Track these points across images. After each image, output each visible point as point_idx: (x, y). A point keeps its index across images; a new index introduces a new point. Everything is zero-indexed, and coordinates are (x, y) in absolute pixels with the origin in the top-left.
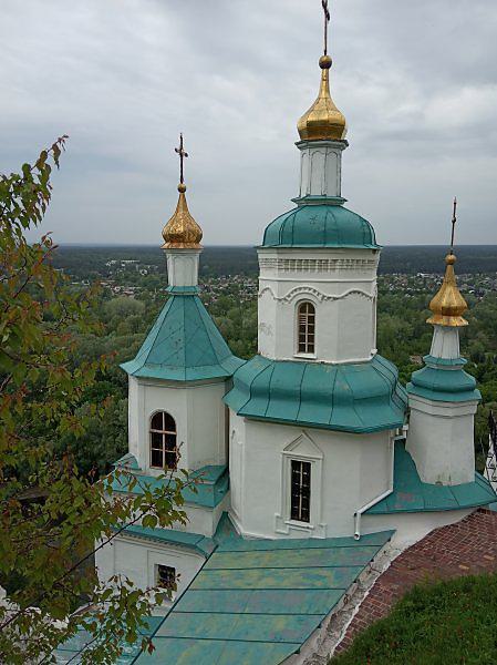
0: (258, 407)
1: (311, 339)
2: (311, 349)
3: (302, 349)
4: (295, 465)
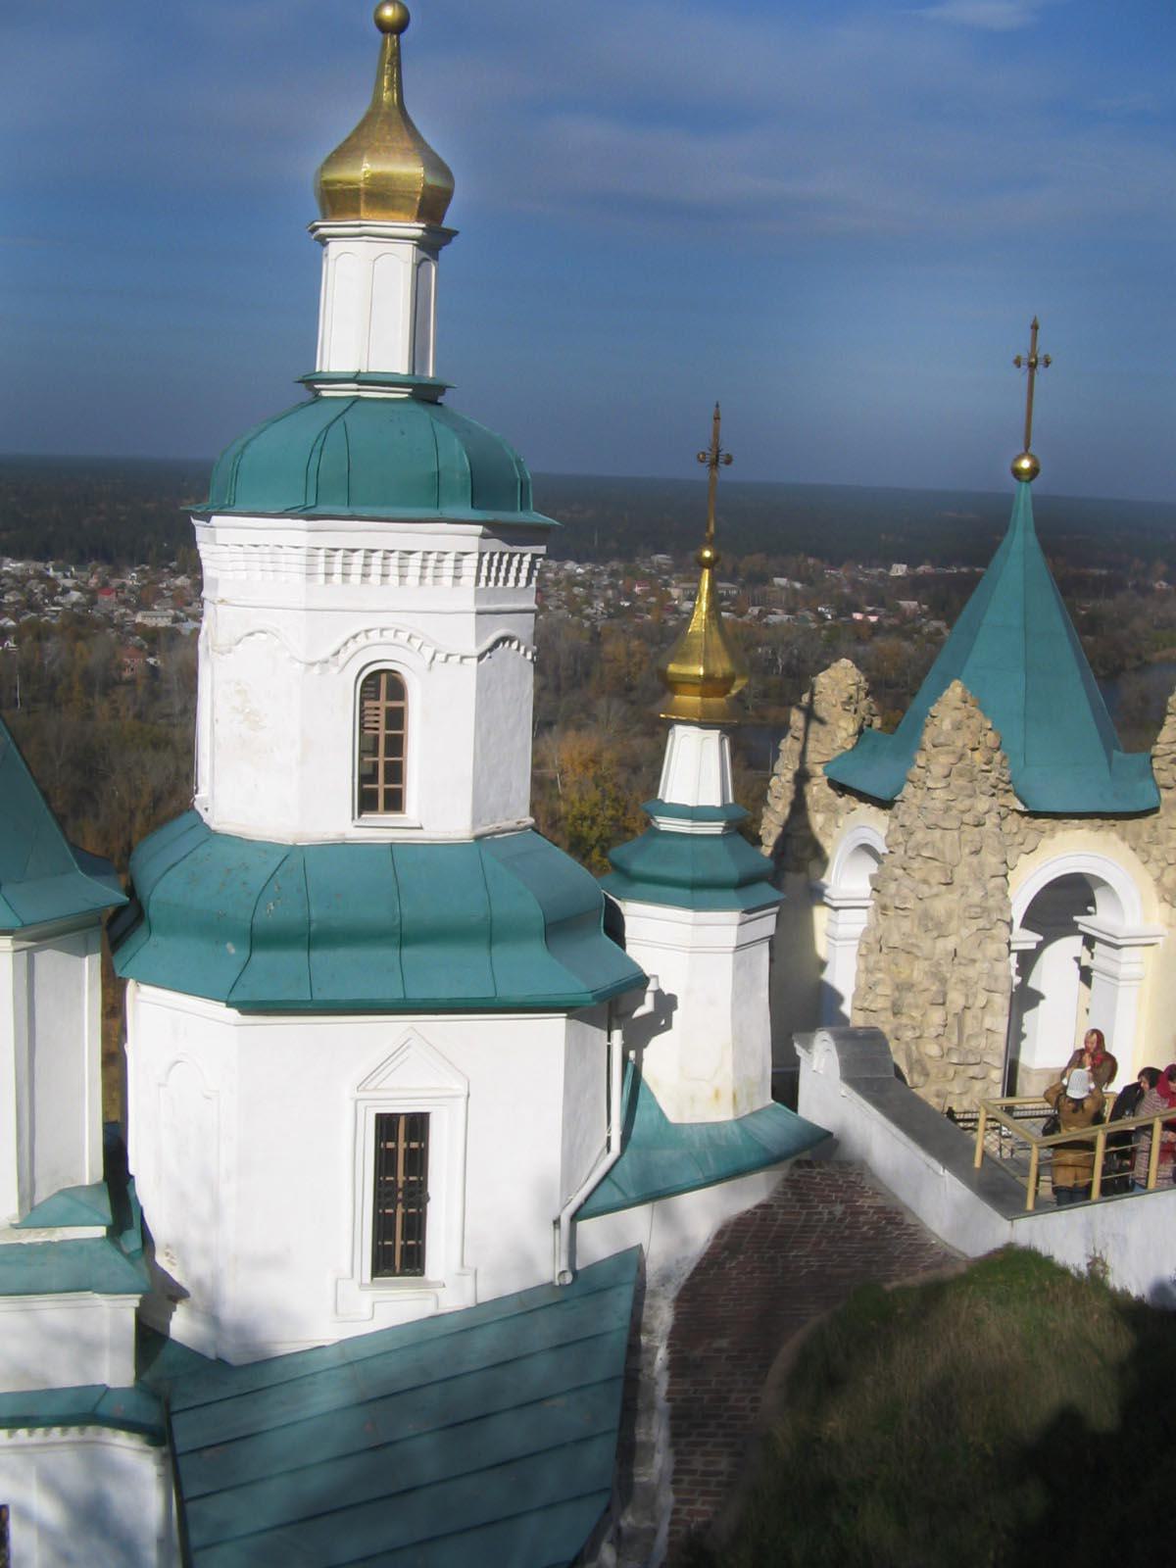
0: (282, 967)
1: (396, 772)
3: (366, 802)
4: (386, 1125)
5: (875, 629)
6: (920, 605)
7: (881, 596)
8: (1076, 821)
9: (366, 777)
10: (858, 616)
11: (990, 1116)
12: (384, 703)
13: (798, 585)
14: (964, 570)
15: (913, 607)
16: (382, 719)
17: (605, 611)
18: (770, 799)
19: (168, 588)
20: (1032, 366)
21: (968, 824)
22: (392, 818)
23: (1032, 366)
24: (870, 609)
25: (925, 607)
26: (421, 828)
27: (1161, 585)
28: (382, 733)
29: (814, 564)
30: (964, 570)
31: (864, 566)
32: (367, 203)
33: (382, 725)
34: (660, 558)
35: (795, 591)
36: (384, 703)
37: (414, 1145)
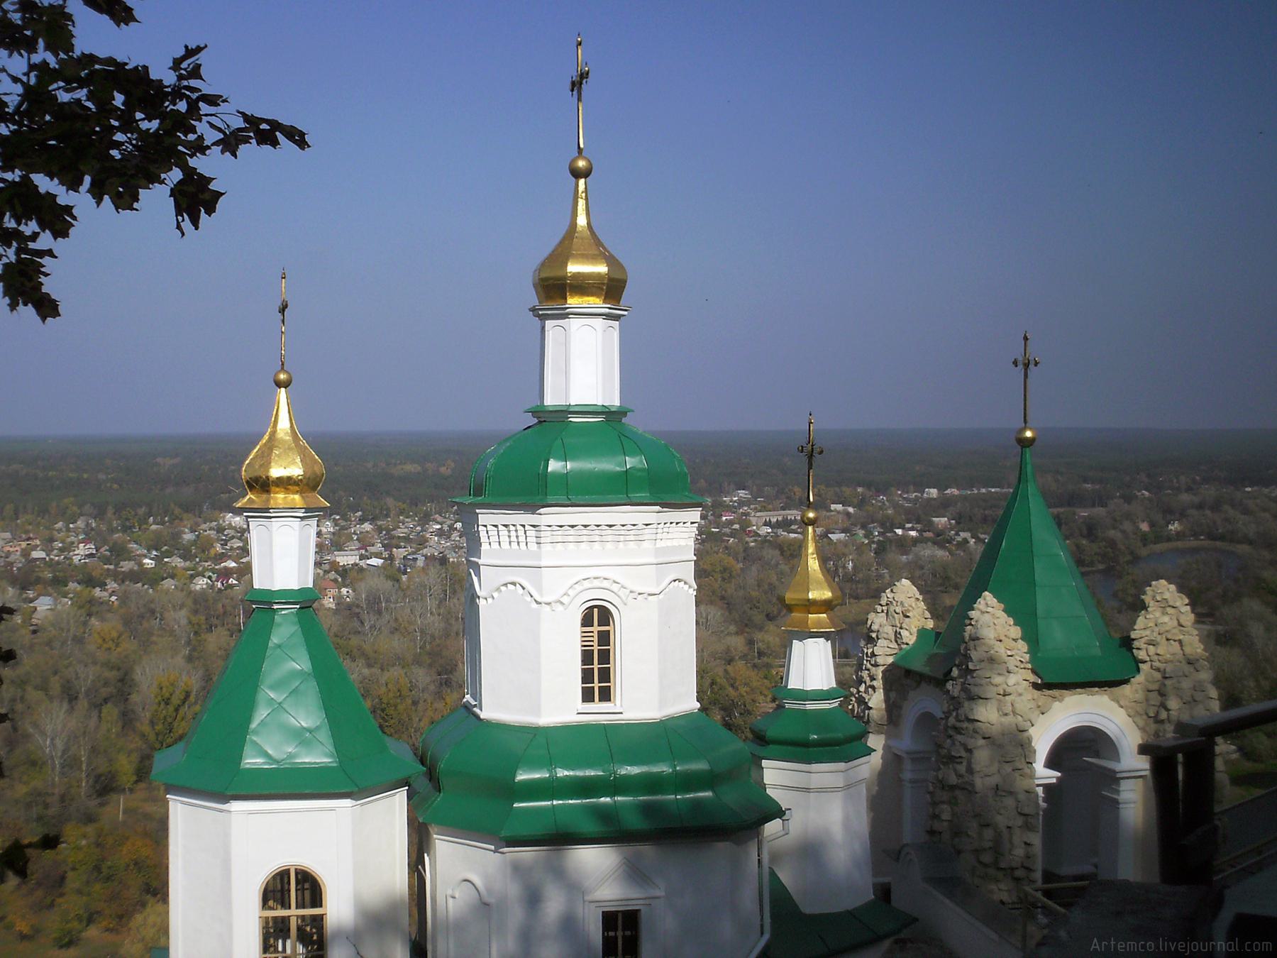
1: (605, 675)
2: (606, 695)
3: (588, 696)
5: (915, 541)
6: (949, 520)
7: (920, 516)
8: (1097, 689)
9: (587, 676)
10: (899, 532)
11: (988, 680)
12: (596, 628)
13: (851, 510)
14: (983, 491)
15: (943, 522)
16: (596, 639)
17: (699, 538)
18: (89, 588)
19: (355, 533)
20: (1026, 366)
21: (1017, 868)
22: (605, 706)
23: (1026, 366)
24: (910, 525)
25: (953, 522)
26: (621, 713)
27: (1143, 494)
28: (596, 648)
29: (863, 493)
30: (983, 491)
31: (903, 491)
32: (570, 291)
33: (595, 644)
34: (742, 493)
35: (848, 514)
36: (596, 628)
37: (612, 934)
